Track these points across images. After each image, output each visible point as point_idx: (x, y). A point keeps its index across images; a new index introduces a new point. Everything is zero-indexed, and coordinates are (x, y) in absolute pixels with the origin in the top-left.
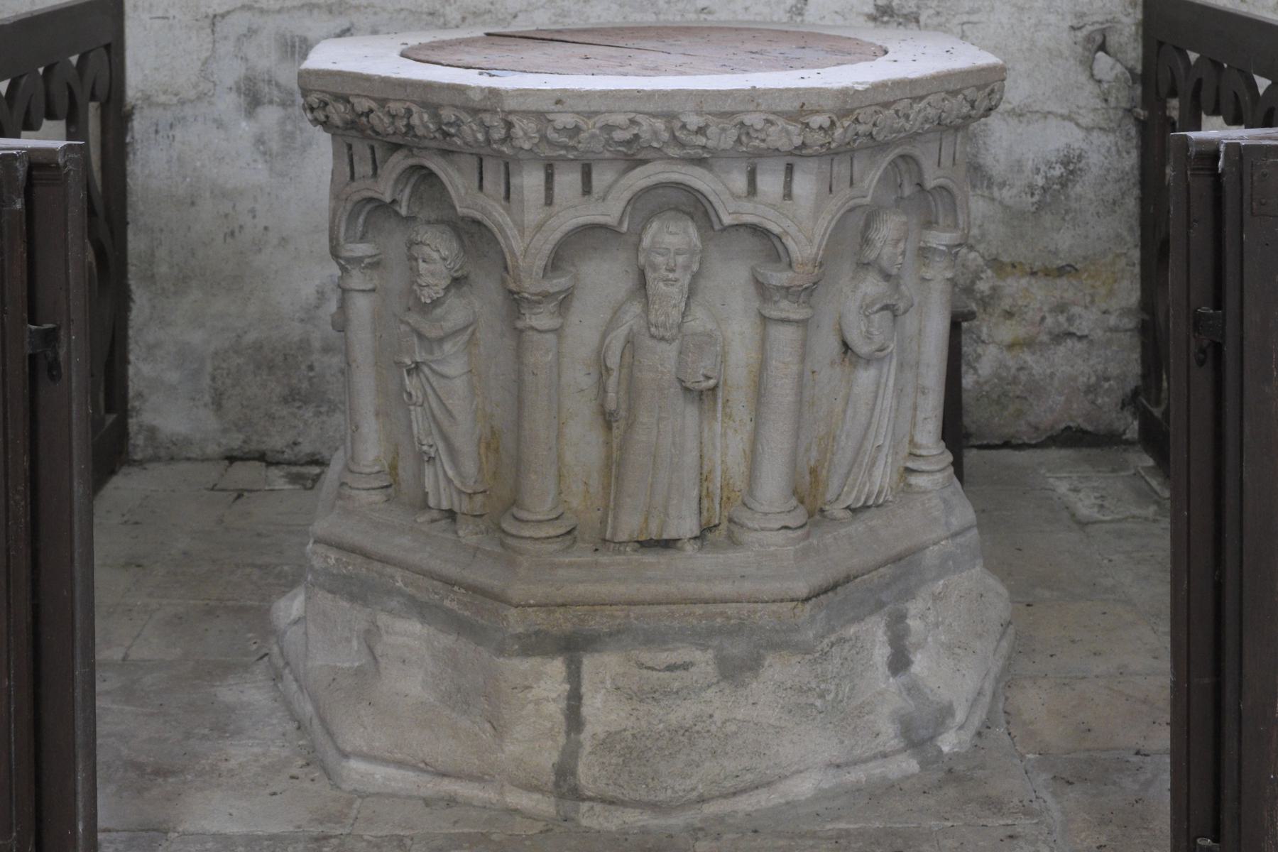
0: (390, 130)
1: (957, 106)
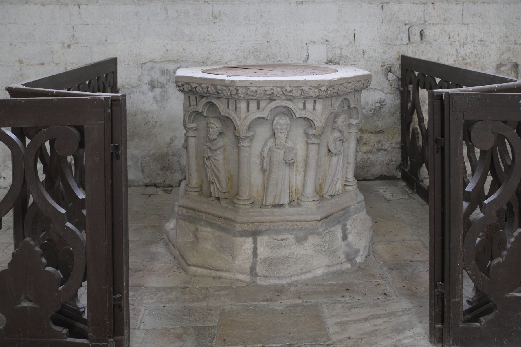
0: (202, 92)
1: (360, 85)
